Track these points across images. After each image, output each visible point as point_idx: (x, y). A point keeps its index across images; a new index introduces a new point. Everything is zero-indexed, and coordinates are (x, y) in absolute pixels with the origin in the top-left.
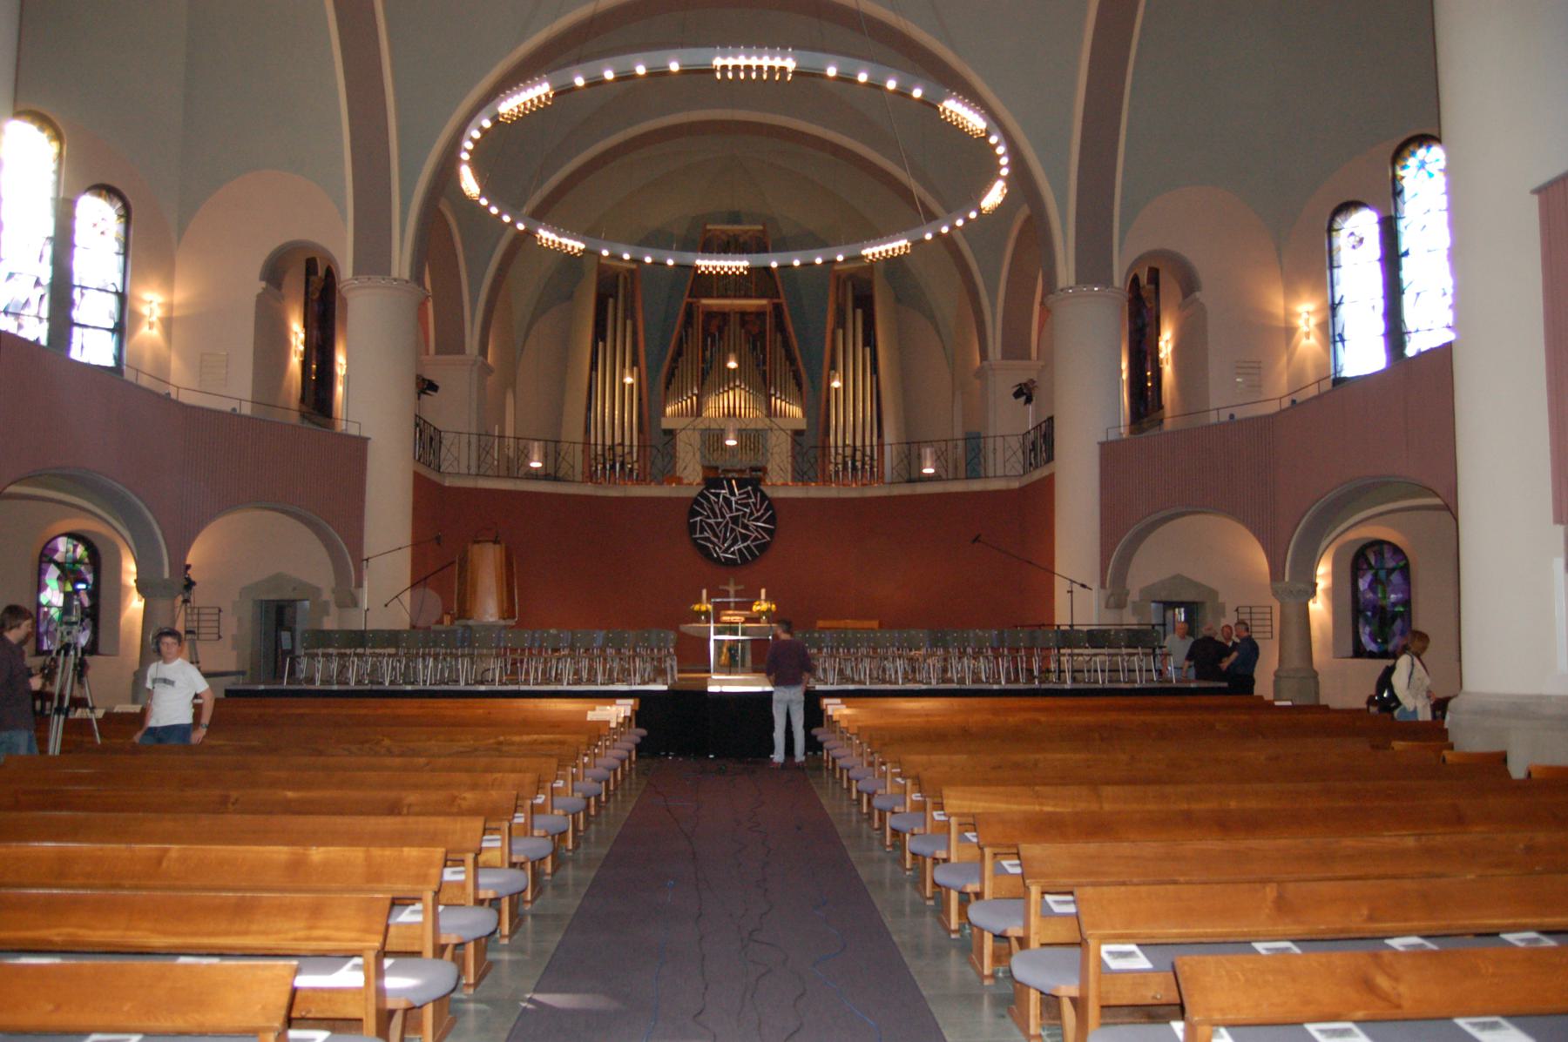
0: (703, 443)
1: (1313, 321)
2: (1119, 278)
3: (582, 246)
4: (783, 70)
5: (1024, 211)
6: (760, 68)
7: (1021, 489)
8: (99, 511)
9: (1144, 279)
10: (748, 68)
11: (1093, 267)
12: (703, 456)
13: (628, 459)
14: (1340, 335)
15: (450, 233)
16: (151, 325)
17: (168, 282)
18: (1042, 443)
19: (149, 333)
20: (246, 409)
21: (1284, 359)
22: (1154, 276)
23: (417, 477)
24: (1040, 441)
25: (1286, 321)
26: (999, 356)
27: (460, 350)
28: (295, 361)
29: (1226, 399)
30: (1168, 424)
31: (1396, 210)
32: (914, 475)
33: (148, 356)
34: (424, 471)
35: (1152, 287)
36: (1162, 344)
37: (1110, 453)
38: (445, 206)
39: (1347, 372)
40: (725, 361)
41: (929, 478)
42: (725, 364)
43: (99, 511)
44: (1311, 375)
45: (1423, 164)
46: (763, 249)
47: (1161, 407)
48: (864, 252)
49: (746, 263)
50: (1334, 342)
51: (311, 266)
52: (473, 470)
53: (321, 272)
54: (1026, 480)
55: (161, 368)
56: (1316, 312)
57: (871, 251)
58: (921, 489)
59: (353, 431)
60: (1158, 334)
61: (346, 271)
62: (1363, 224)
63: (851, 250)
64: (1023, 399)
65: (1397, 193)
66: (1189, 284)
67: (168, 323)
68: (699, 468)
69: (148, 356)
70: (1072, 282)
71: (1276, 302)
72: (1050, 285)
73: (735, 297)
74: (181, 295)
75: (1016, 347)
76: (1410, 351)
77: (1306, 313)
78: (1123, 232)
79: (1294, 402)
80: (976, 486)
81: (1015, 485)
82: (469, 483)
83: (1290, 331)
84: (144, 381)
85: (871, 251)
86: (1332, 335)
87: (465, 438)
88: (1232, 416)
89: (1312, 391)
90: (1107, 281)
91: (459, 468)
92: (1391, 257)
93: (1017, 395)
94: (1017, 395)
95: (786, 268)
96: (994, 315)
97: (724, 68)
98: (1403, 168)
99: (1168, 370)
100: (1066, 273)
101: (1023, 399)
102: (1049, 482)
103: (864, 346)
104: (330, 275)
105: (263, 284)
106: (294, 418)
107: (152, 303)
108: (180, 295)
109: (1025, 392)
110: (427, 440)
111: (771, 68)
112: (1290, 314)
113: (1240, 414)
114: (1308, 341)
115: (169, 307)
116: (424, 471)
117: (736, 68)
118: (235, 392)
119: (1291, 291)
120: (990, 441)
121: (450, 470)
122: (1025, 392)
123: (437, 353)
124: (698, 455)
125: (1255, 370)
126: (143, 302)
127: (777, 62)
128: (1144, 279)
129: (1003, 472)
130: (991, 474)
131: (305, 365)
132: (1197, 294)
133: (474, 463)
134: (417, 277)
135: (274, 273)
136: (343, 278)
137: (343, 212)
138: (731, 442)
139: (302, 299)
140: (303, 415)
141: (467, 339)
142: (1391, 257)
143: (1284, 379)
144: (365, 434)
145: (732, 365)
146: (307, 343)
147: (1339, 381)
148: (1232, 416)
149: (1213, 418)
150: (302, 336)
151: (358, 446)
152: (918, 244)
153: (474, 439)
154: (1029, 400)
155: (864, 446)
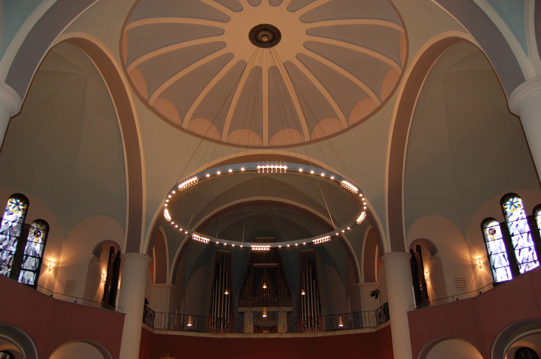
0: (254, 317)
1: (482, 262)
2: (407, 250)
3: (209, 240)
4: (283, 169)
5: (370, 227)
6: (274, 169)
7: (376, 332)
8: (16, 343)
9: (415, 251)
10: (270, 169)
11: (398, 246)
12: (254, 322)
13: (226, 323)
14: (493, 267)
15: (163, 236)
16: (50, 270)
17: (58, 255)
18: (384, 312)
19: (48, 273)
20: (80, 302)
21: (473, 276)
22: (419, 248)
23: (143, 330)
24: (382, 313)
25: (472, 262)
26: (363, 281)
27: (165, 282)
28: (102, 285)
29: (452, 294)
30: (432, 303)
31: (506, 220)
32: (335, 328)
33: (47, 281)
34: (146, 327)
35: (418, 253)
36: (425, 274)
37: (410, 315)
38: (161, 229)
39: (499, 280)
40: (262, 285)
41: (341, 329)
42: (262, 287)
43: (16, 343)
44: (485, 283)
45: (512, 204)
46: (275, 241)
47: (427, 297)
48: (313, 241)
49: (269, 246)
50: (491, 270)
51: (112, 249)
52: (166, 328)
53: (116, 252)
54: (379, 328)
55: (51, 284)
56: (482, 258)
57: (317, 241)
58: (338, 333)
59: (120, 311)
60: (423, 270)
61: (123, 251)
62: (495, 225)
63: (309, 240)
64: (375, 297)
65: (505, 214)
66: (433, 251)
67: (56, 269)
68: (252, 326)
69: (47, 281)
70: (390, 251)
71: (467, 255)
72: (381, 252)
73: (266, 263)
74: (62, 259)
75: (370, 278)
76: (522, 271)
77: (479, 259)
78: (407, 231)
79: (480, 293)
80: (359, 331)
81: (374, 330)
82: (164, 333)
83: (474, 266)
84: (44, 291)
85: (317, 241)
86: (491, 268)
87: (164, 315)
88: (457, 299)
89: (486, 289)
90: (404, 251)
91: (161, 326)
92: (507, 237)
93: (372, 295)
94: (372, 295)
95: (284, 248)
96: (360, 265)
97: (261, 169)
98: (505, 205)
99: (429, 283)
100: (387, 247)
101: (375, 297)
102: (389, 327)
103: (313, 279)
104: (119, 252)
105: (93, 255)
106: (99, 306)
107: (51, 261)
108: (62, 259)
109: (375, 294)
110: (148, 315)
111: (278, 169)
112: (472, 260)
113: (461, 298)
114: (481, 269)
115: (58, 263)
116: (146, 327)
117: (265, 169)
118: (79, 295)
119: (471, 251)
120: (363, 313)
121: (158, 327)
122: (375, 294)
123: (156, 283)
124: (252, 321)
125: (462, 283)
126: (48, 261)
127: (281, 167)
128: (415, 251)
129: (369, 325)
130: (364, 326)
131: (106, 286)
132: (437, 254)
133: (166, 326)
134: (150, 253)
135: (97, 252)
136: (122, 254)
137: (124, 230)
138: (265, 316)
139: (107, 261)
140: (103, 305)
141: (167, 277)
142: (507, 237)
143: (475, 284)
144: (124, 312)
145: (265, 287)
146: (107, 278)
147: (496, 284)
148: (457, 299)
149: (450, 300)
150: (106, 275)
151: (122, 317)
152: (333, 237)
153: (167, 315)
154: (377, 297)
155: (314, 317)
